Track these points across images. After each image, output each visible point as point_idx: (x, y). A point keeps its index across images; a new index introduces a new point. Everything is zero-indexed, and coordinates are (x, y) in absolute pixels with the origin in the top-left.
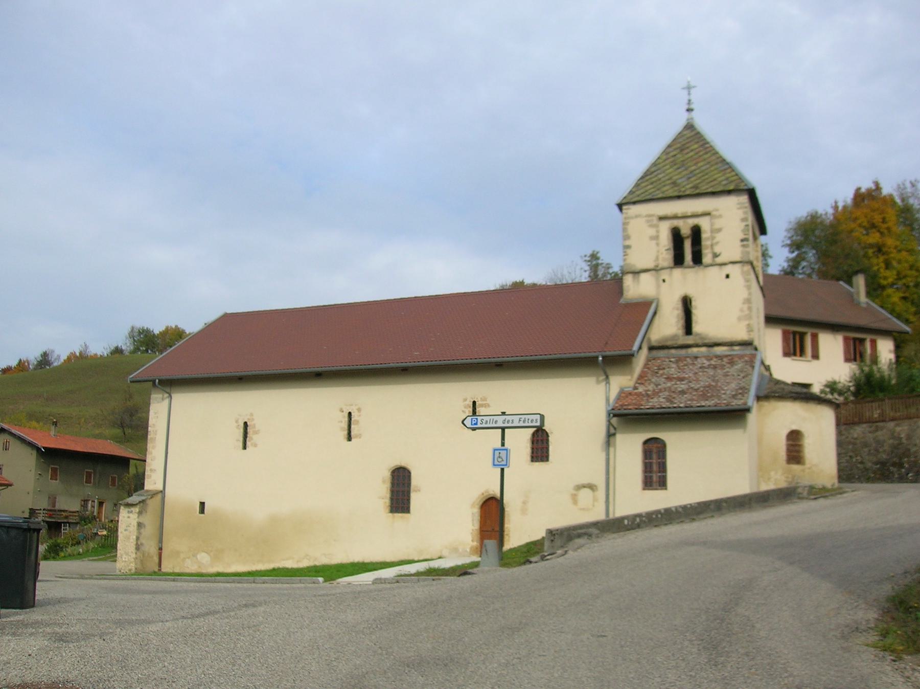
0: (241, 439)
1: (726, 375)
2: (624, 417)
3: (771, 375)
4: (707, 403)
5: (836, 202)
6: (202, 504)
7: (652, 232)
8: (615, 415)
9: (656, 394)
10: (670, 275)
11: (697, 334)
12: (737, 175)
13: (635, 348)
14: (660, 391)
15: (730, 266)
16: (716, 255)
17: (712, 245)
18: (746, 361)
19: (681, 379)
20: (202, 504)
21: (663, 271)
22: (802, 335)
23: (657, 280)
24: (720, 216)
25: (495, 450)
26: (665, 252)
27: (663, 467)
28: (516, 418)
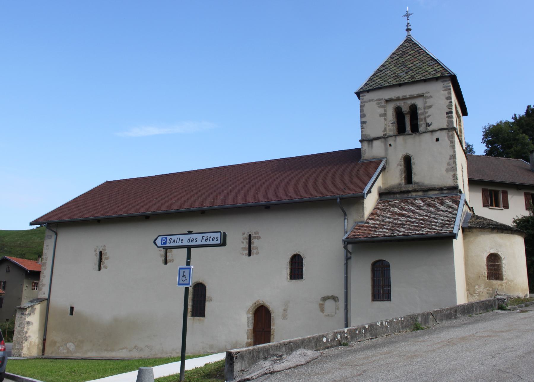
0: (98, 263)
1: (437, 211)
2: (356, 245)
3: (473, 213)
4: (421, 232)
5: (515, 115)
6: (72, 308)
7: (381, 111)
8: (349, 243)
9: (382, 226)
10: (395, 141)
11: (416, 183)
12: (442, 67)
13: (366, 191)
14: (385, 224)
15: (439, 132)
16: (428, 125)
17: (425, 118)
18: (453, 201)
19: (402, 215)
20: (72, 308)
21: (390, 138)
22: (496, 193)
23: (385, 145)
24: (431, 97)
25: (180, 269)
26: (391, 125)
27: (388, 285)
28: (199, 236)
